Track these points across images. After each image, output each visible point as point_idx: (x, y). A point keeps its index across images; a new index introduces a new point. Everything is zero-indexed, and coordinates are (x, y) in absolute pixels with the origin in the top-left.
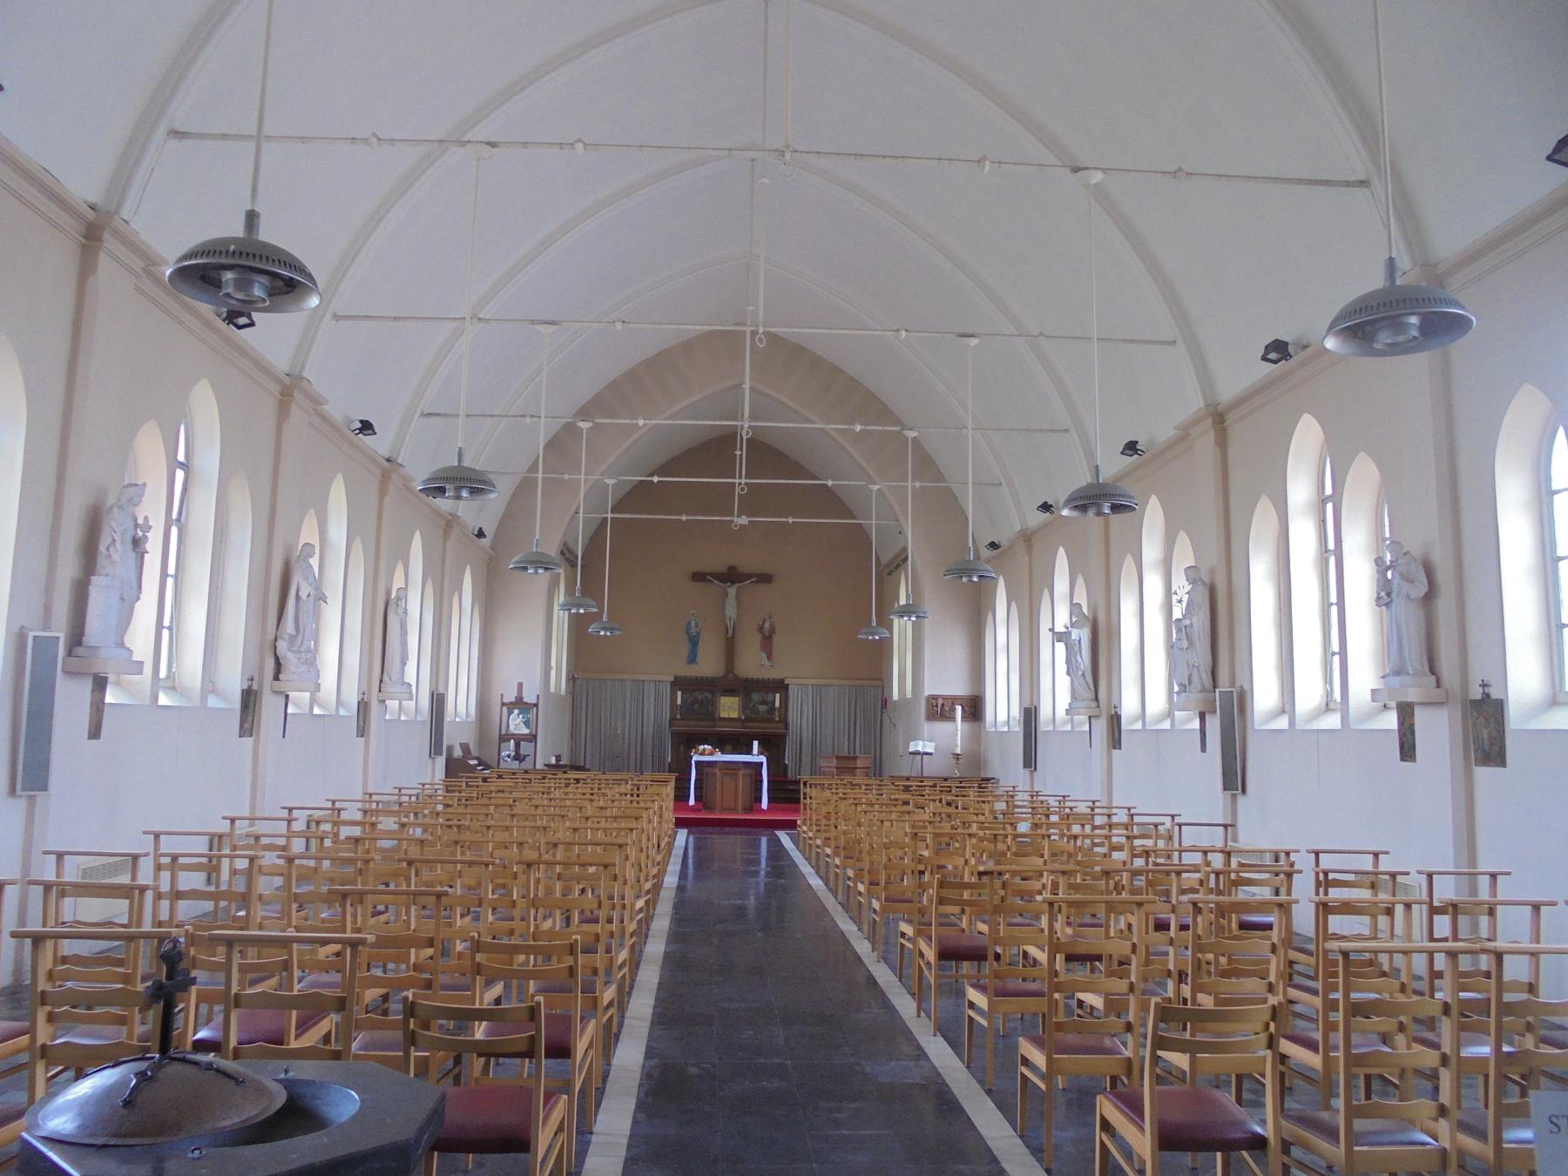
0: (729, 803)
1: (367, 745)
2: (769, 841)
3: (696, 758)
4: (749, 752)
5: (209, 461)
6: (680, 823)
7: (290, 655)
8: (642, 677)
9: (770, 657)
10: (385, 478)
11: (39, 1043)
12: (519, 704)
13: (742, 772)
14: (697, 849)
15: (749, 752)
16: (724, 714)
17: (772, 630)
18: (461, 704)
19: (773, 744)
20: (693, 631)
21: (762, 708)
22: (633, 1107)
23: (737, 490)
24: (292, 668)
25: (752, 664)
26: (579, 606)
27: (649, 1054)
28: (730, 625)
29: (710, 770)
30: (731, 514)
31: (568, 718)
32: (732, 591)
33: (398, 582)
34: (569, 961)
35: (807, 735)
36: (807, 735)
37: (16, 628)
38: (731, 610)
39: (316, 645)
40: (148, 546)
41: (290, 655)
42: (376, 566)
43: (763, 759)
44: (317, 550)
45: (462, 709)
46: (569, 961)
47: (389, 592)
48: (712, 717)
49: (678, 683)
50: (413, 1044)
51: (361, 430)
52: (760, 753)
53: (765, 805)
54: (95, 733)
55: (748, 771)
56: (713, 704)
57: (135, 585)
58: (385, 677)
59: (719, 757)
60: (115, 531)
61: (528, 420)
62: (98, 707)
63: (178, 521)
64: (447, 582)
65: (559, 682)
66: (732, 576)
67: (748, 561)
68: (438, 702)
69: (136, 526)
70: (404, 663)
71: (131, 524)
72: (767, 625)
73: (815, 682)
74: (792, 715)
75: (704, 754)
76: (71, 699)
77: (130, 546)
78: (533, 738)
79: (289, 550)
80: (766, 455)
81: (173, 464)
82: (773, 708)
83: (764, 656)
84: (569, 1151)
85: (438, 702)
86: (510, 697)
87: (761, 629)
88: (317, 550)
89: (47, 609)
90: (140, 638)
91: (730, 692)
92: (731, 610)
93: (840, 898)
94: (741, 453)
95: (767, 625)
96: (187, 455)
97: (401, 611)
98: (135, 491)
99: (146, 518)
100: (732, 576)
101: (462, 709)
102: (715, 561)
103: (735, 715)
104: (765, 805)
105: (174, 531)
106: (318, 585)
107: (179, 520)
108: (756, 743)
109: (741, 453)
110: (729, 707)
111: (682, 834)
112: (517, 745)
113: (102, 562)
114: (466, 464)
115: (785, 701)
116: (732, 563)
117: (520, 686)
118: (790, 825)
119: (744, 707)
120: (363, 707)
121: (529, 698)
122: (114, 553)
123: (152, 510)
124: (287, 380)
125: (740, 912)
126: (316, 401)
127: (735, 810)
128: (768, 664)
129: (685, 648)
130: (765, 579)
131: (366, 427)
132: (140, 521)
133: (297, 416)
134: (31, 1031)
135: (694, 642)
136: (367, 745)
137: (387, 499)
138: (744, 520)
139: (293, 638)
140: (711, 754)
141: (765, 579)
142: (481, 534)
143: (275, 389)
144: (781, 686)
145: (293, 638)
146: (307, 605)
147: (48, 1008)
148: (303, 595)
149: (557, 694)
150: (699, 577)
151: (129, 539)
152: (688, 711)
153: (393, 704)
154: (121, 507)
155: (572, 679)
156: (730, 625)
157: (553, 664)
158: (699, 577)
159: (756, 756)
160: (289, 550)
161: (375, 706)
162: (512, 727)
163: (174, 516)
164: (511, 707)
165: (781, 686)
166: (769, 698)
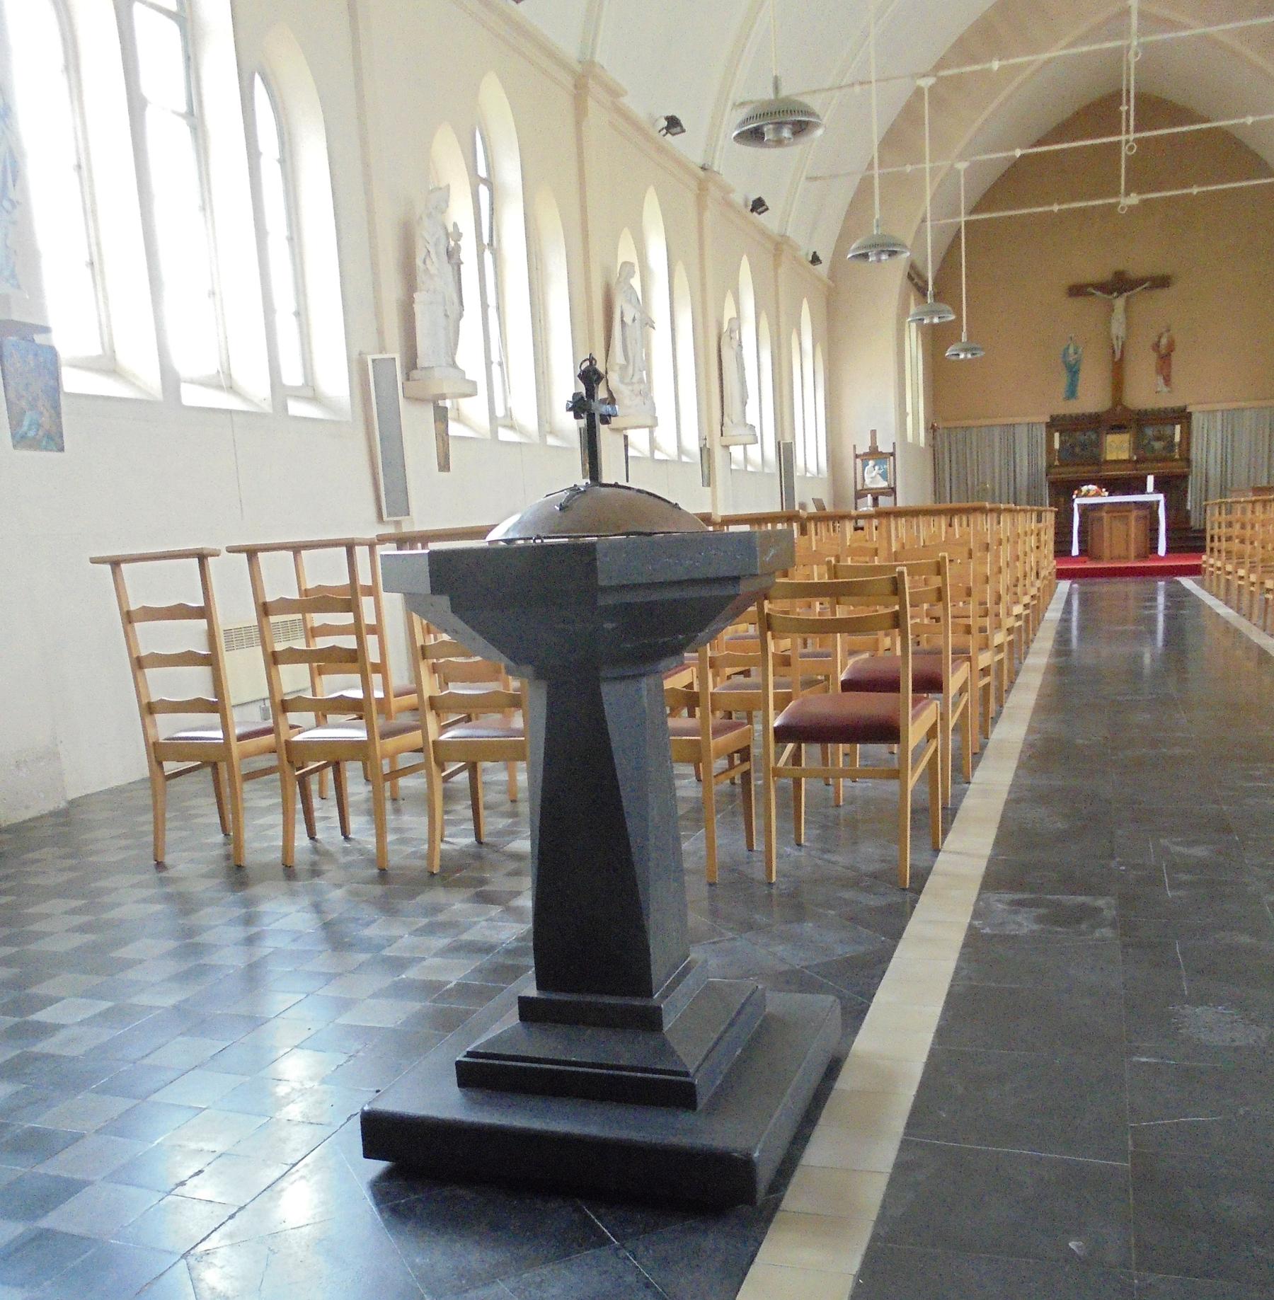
0: (1119, 544)
1: (714, 494)
2: (1169, 596)
3: (1077, 501)
4: (1143, 490)
5: (510, 174)
6: (1061, 574)
7: (623, 388)
8: (1010, 420)
9: (1167, 381)
10: (702, 188)
11: (426, 695)
12: (874, 453)
13: (1134, 513)
14: (1084, 602)
15: (1143, 490)
16: (1111, 456)
17: (1171, 347)
18: (811, 457)
19: (1172, 485)
20: (1072, 358)
21: (1158, 445)
22: (1015, 766)
23: (1124, 149)
24: (627, 402)
25: (1145, 392)
26: (932, 313)
27: (1031, 730)
28: (1118, 345)
29: (1096, 514)
30: (1116, 194)
31: (930, 471)
32: (1120, 303)
33: (729, 313)
34: (936, 581)
35: (1215, 473)
36: (1215, 473)
37: (355, 356)
38: (1118, 328)
39: (649, 375)
40: (463, 256)
41: (623, 388)
42: (703, 285)
43: (1161, 497)
44: (637, 268)
45: (812, 467)
46: (936, 581)
47: (720, 325)
48: (1097, 461)
49: (1055, 424)
50: (769, 628)
51: (668, 128)
52: (1158, 489)
53: (1162, 550)
54: (444, 466)
55: (1141, 513)
56: (1098, 444)
57: (456, 300)
58: (726, 419)
59: (1105, 498)
60: (426, 237)
61: (857, 89)
62: (443, 438)
63: (490, 245)
64: (783, 319)
65: (916, 431)
66: (1120, 284)
67: (1140, 263)
68: (785, 453)
69: (447, 235)
70: (744, 403)
71: (441, 233)
72: (1164, 341)
73: (1224, 406)
74: (1196, 453)
75: (1090, 496)
76: (416, 427)
77: (445, 258)
78: (892, 491)
79: (607, 271)
80: (1154, 109)
81: (475, 180)
82: (1171, 445)
83: (1161, 381)
84: (944, 760)
85: (785, 453)
86: (864, 448)
87: (1156, 346)
88: (637, 268)
89: (380, 332)
90: (469, 357)
91: (1118, 428)
92: (1118, 328)
93: (1255, 619)
94: (1128, 108)
95: (1164, 341)
96: (489, 167)
97: (735, 344)
98: (441, 197)
99: (455, 225)
100: (1120, 284)
101: (812, 467)
102: (1094, 269)
103: (1125, 456)
104: (1162, 550)
105: (488, 256)
106: (643, 306)
107: (491, 244)
108: (1150, 480)
109: (1128, 108)
110: (1117, 447)
111: (1064, 586)
112: (875, 500)
113: (421, 277)
114: (785, 92)
115: (1187, 434)
116: (1121, 268)
117: (874, 433)
118: (1194, 571)
119: (1137, 446)
120: (706, 452)
121: (884, 447)
122: (432, 268)
123: (460, 212)
124: (578, 68)
125: (1135, 673)
126: (614, 92)
127: (1126, 558)
128: (1165, 389)
129: (1064, 379)
130: (1162, 282)
131: (673, 124)
132: (451, 229)
133: (597, 116)
134: (422, 727)
135: (1073, 371)
136: (714, 494)
137: (708, 215)
138: (1134, 199)
139: (624, 368)
140: (1097, 494)
141: (1162, 282)
142: (815, 259)
143: (568, 81)
144: (1182, 416)
145: (624, 368)
146: (634, 331)
147: (431, 661)
148: (628, 319)
149: (915, 445)
150: (1077, 291)
151: (443, 251)
152: (1068, 455)
153: (737, 451)
154: (430, 216)
155: (932, 429)
156: (1118, 345)
157: (909, 409)
158: (1077, 291)
159: (1151, 495)
160: (607, 271)
161: (718, 453)
162: (867, 481)
163: (486, 240)
164: (865, 458)
165: (1182, 416)
166: (1168, 431)
